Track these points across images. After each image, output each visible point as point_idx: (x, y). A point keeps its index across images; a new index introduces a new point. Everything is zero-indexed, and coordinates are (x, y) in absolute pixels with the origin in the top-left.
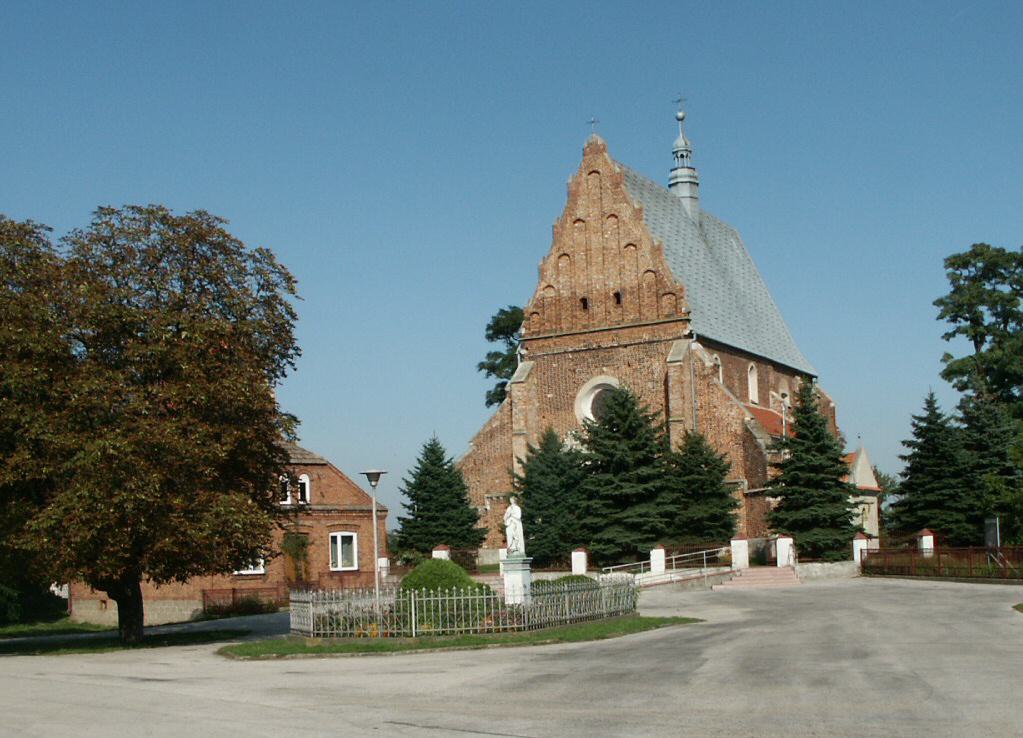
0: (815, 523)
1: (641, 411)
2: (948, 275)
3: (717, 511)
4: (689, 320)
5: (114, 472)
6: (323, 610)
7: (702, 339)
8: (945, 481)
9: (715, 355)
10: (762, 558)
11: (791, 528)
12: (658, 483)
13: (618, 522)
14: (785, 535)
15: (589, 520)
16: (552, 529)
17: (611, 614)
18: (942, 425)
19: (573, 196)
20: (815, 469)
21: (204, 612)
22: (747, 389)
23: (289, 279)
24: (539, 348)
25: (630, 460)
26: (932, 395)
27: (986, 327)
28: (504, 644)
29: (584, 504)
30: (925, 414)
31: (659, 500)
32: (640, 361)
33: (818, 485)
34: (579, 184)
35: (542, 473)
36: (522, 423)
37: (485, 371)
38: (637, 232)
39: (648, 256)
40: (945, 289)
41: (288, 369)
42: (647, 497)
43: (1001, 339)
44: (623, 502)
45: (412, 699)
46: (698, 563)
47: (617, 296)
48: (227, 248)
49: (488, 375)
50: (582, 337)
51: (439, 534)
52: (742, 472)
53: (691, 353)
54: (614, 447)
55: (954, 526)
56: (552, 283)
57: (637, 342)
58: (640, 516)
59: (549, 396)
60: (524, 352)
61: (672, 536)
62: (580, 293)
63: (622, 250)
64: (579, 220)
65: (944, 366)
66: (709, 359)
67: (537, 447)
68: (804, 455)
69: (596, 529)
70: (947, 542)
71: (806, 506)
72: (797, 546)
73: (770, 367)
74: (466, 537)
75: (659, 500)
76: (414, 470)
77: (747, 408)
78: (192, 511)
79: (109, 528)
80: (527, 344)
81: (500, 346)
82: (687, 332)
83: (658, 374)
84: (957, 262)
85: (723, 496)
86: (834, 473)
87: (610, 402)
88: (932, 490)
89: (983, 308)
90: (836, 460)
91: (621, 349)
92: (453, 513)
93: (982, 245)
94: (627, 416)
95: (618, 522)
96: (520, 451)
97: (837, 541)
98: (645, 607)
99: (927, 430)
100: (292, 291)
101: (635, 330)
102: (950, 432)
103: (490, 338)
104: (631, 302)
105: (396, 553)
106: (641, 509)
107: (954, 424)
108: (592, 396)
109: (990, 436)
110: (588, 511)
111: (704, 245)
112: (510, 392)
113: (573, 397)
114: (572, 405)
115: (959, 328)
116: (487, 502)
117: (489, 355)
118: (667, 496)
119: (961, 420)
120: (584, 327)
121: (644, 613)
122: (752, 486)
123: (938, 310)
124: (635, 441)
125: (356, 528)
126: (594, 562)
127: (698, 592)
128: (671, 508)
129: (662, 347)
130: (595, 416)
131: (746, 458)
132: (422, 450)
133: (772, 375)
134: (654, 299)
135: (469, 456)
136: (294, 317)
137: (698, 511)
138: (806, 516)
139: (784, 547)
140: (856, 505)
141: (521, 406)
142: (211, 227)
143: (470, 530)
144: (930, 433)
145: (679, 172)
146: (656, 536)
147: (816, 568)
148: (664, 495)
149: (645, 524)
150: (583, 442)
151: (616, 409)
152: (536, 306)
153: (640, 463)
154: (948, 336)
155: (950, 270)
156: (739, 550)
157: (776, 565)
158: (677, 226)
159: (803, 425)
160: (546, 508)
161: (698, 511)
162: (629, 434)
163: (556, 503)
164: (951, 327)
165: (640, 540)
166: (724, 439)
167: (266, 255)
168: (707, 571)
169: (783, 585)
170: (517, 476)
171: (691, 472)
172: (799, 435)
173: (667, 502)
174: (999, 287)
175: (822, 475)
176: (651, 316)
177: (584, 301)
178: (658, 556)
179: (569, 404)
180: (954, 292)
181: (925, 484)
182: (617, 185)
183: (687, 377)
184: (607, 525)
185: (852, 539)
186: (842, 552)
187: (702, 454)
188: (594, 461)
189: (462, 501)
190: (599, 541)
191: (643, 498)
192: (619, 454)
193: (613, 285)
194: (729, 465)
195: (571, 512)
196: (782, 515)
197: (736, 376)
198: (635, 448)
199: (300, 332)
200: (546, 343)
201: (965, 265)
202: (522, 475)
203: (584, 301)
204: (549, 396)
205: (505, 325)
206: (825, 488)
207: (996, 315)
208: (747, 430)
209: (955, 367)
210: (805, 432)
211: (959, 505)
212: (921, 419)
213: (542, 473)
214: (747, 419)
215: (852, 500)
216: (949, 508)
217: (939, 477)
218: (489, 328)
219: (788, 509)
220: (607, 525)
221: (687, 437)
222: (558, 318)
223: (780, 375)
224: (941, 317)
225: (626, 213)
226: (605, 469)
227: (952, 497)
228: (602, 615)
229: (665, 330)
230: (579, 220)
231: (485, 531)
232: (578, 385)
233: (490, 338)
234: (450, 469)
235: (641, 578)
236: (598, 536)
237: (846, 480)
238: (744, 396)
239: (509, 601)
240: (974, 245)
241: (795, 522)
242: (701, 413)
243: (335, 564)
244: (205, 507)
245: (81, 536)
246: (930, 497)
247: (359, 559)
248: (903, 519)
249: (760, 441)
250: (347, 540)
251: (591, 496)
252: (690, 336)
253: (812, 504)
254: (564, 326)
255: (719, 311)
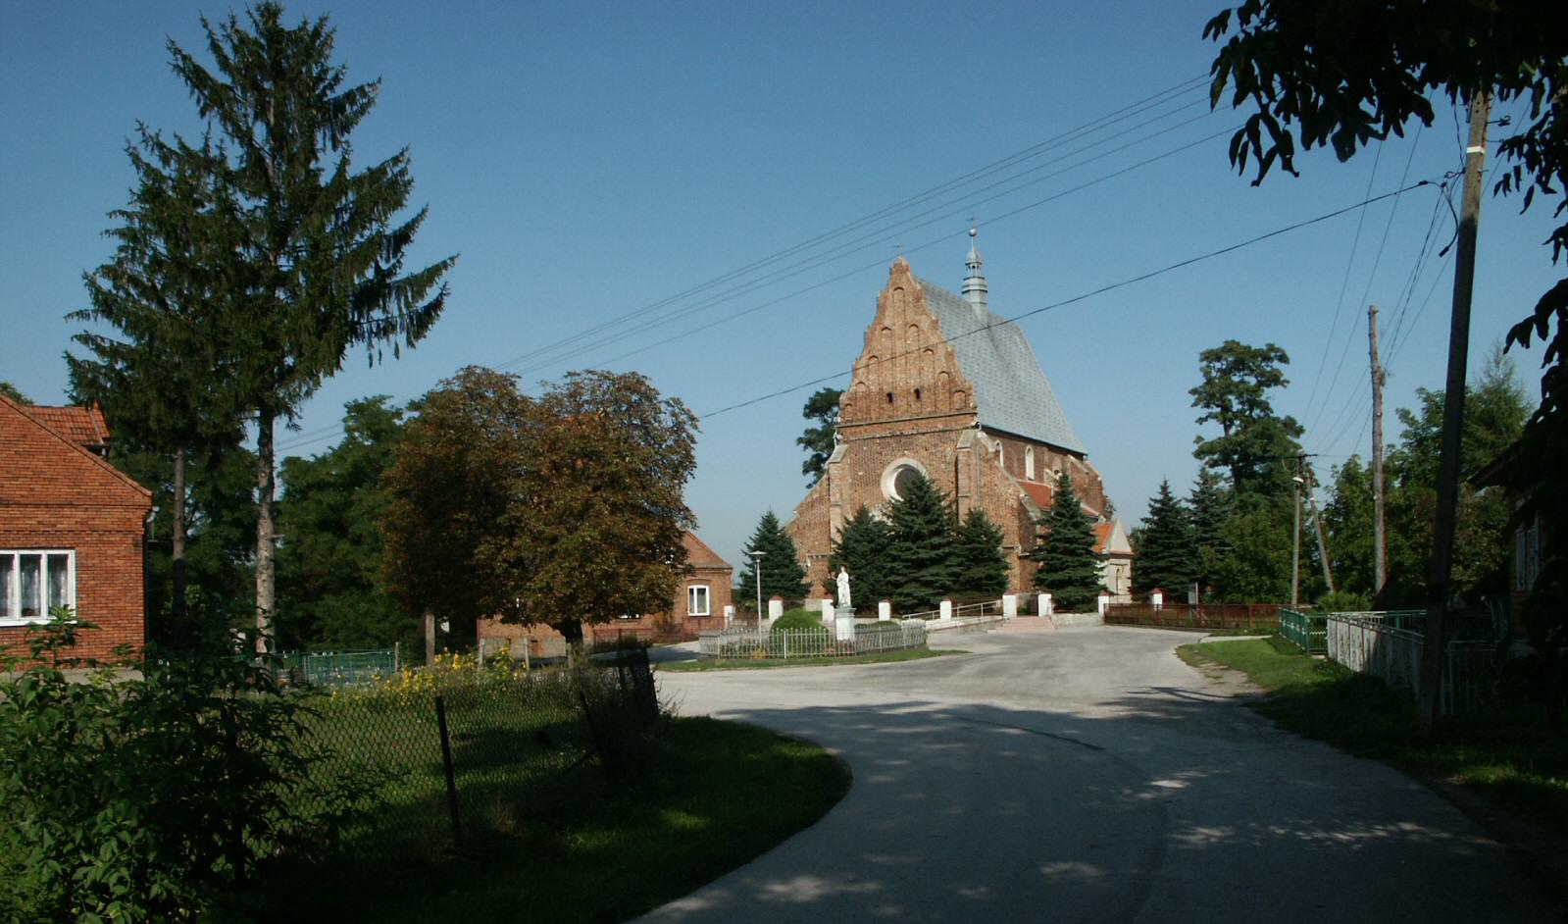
0: (1069, 582)
1: (935, 493)
2: (1201, 369)
3: (993, 572)
4: (975, 414)
5: (587, 553)
6: (725, 643)
7: (988, 430)
8: (1173, 551)
9: (998, 441)
10: (1029, 609)
11: (1050, 587)
12: (947, 550)
13: (916, 580)
14: (1047, 592)
15: (892, 578)
16: (863, 585)
17: (909, 647)
18: (1173, 506)
19: (881, 308)
20: (1069, 541)
21: (595, 646)
22: (1024, 468)
23: (692, 419)
24: (852, 434)
25: (925, 531)
26: (1166, 482)
27: (1234, 413)
28: (843, 663)
29: (889, 565)
30: (1160, 497)
31: (947, 563)
32: (935, 446)
33: (1072, 553)
34: (886, 298)
35: (857, 541)
36: (838, 496)
37: (802, 445)
38: (934, 340)
39: (943, 360)
40: (1199, 381)
41: (689, 478)
42: (939, 561)
43: (1248, 422)
44: (920, 564)
46: (977, 613)
47: (917, 392)
48: (649, 396)
49: (805, 448)
50: (888, 426)
51: (774, 587)
52: (1016, 538)
53: (977, 441)
54: (913, 521)
55: (1179, 587)
56: (863, 379)
58: (933, 575)
60: (839, 437)
61: (957, 591)
62: (887, 389)
64: (886, 328)
65: (1196, 447)
66: (991, 445)
67: (851, 519)
68: (1061, 530)
69: (898, 585)
70: (1173, 598)
71: (1062, 569)
72: (1053, 600)
73: (1045, 449)
74: (793, 590)
75: (947, 563)
76: (754, 537)
77: (1023, 485)
78: (632, 576)
79: (582, 586)
80: (842, 430)
81: (816, 423)
82: (974, 424)
83: (950, 457)
84: (1211, 356)
85: (998, 560)
86: (1085, 543)
87: (910, 485)
88: (1163, 558)
89: (1232, 397)
90: (1088, 534)
92: (785, 571)
93: (1233, 341)
94: (923, 497)
95: (916, 580)
96: (837, 522)
97: (1085, 597)
98: (934, 645)
99: (1161, 510)
100: (696, 427)
101: (931, 420)
102: (1179, 512)
103: (807, 416)
104: (929, 397)
105: (739, 602)
106: (934, 570)
107: (1184, 505)
108: (896, 474)
109: (1212, 515)
110: (892, 571)
111: (991, 345)
112: (828, 471)
113: (880, 475)
115: (1211, 413)
116: (808, 560)
117: (807, 432)
118: (954, 560)
119: (1190, 501)
120: (890, 417)
121: (931, 648)
122: (1024, 551)
123: (1193, 398)
124: (929, 517)
125: (708, 582)
126: (897, 610)
127: (977, 635)
128: (957, 570)
129: (953, 436)
130: (899, 494)
131: (1020, 528)
132: (760, 520)
133: (1047, 455)
134: (947, 395)
135: (794, 522)
136: (693, 442)
137: (978, 572)
138: (1061, 577)
139: (1045, 601)
140: (1102, 569)
141: (837, 482)
142: (643, 383)
143: (798, 585)
144: (1165, 510)
145: (971, 281)
146: (945, 592)
147: (1069, 617)
148: (952, 559)
149: (936, 582)
150: (889, 517)
151: (910, 482)
152: (849, 399)
153: (933, 534)
154: (1201, 421)
155: (1205, 363)
156: (1010, 603)
157: (1037, 614)
159: (1062, 506)
160: (859, 569)
161: (978, 572)
162: (926, 511)
163: (867, 564)
164: (1204, 412)
165: (932, 595)
166: (1002, 512)
167: (678, 402)
168: (988, 618)
169: (1042, 630)
170: (835, 543)
171: (973, 542)
172: (1057, 514)
173: (954, 565)
174: (1247, 378)
175: (1075, 546)
176: (944, 409)
177: (890, 395)
178: (946, 606)
179: (875, 481)
180: (1207, 383)
181: (1157, 553)
182: (918, 300)
183: (974, 461)
184: (907, 582)
185: (1097, 596)
186: (1089, 605)
187: (982, 527)
188: (897, 533)
189: (792, 561)
190: (900, 595)
191: (935, 561)
192: (916, 527)
193: (914, 383)
194: (1002, 537)
195: (879, 571)
196: (1043, 576)
197: (1015, 457)
198: (930, 522)
199: (697, 452)
201: (1218, 359)
202: (840, 542)
203: (890, 395)
205: (823, 404)
206: (1077, 555)
207: (1242, 403)
208: (1021, 504)
209: (1205, 449)
210: (1064, 511)
211: (1183, 570)
212: (1156, 501)
213: (857, 541)
214: (1022, 495)
215: (1099, 565)
216: (1176, 572)
217: (1168, 547)
218: (806, 407)
219: (1048, 571)
220: (907, 582)
221: (971, 513)
222: (868, 409)
223: (1053, 454)
224: (1195, 405)
225: (925, 324)
226: (906, 537)
227: (1178, 564)
228: (902, 648)
229: (956, 422)
230: (886, 328)
231: (810, 585)
232: (884, 465)
233: (807, 416)
234: (783, 537)
235: (930, 624)
236: (899, 591)
237: (1094, 549)
238: (1022, 474)
239: (840, 638)
240: (1226, 342)
241: (1053, 582)
242: (984, 490)
243: (692, 610)
244: (640, 574)
245: (561, 592)
246: (1161, 563)
247: (711, 606)
248: (1140, 580)
249: (1031, 514)
250: (702, 592)
251: (895, 559)
252: (976, 426)
253: (1067, 567)
254: (873, 416)
255: (1002, 402)
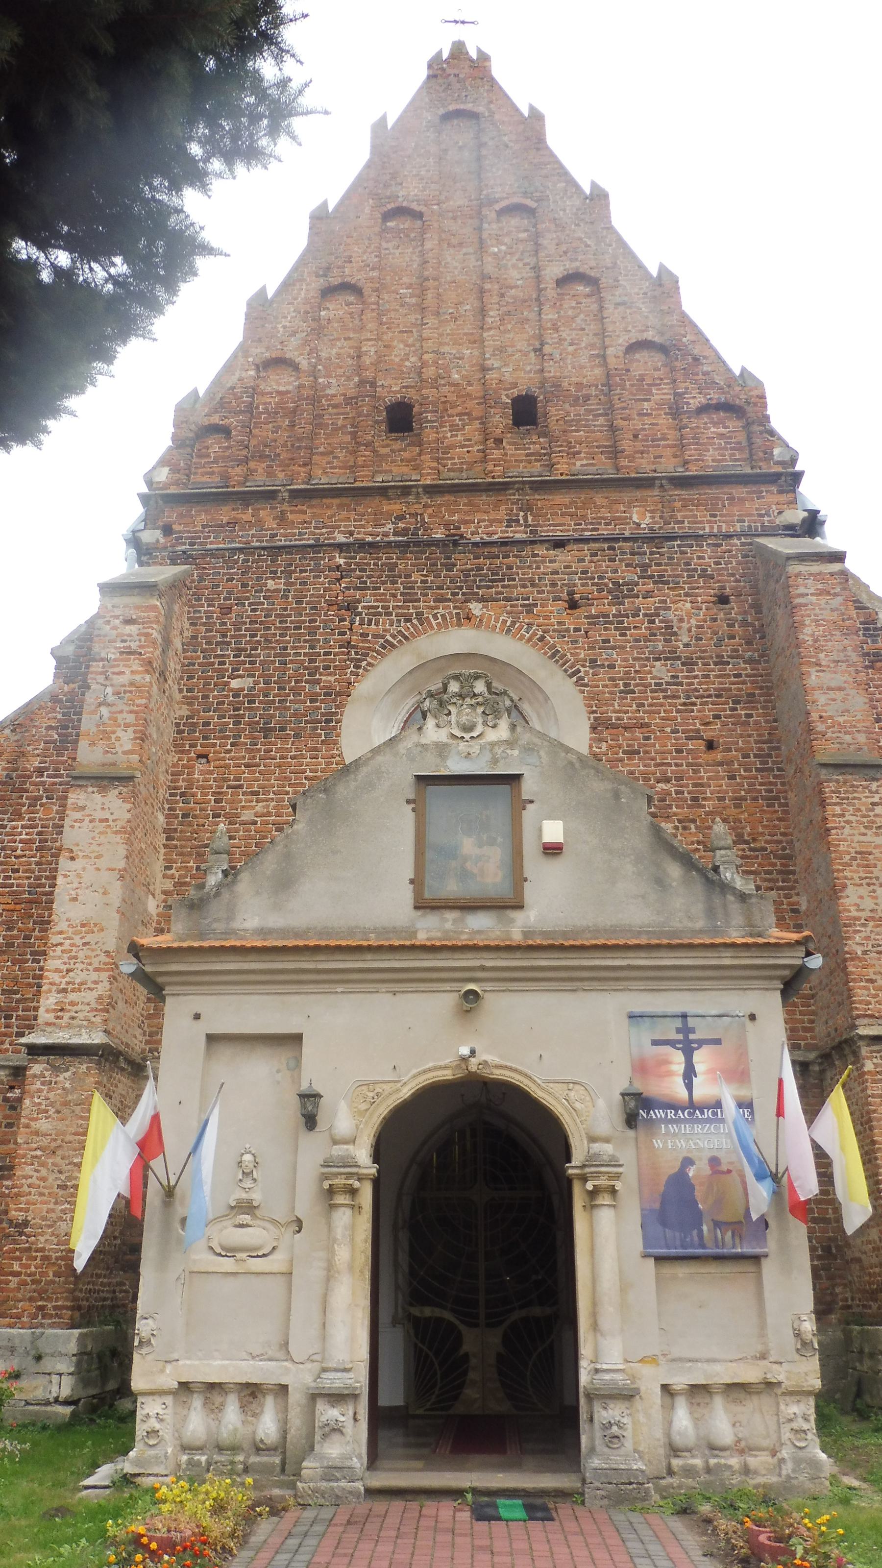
45: (197, 406)
50: (396, 507)
57: (604, 531)
59: (235, 684)
62: (392, 389)
63: (551, 292)
91: (542, 551)
113: (341, 694)
114: (331, 722)
158: (326, 668)
200: (247, 515)
204: (235, 684)
232: (359, 656)
